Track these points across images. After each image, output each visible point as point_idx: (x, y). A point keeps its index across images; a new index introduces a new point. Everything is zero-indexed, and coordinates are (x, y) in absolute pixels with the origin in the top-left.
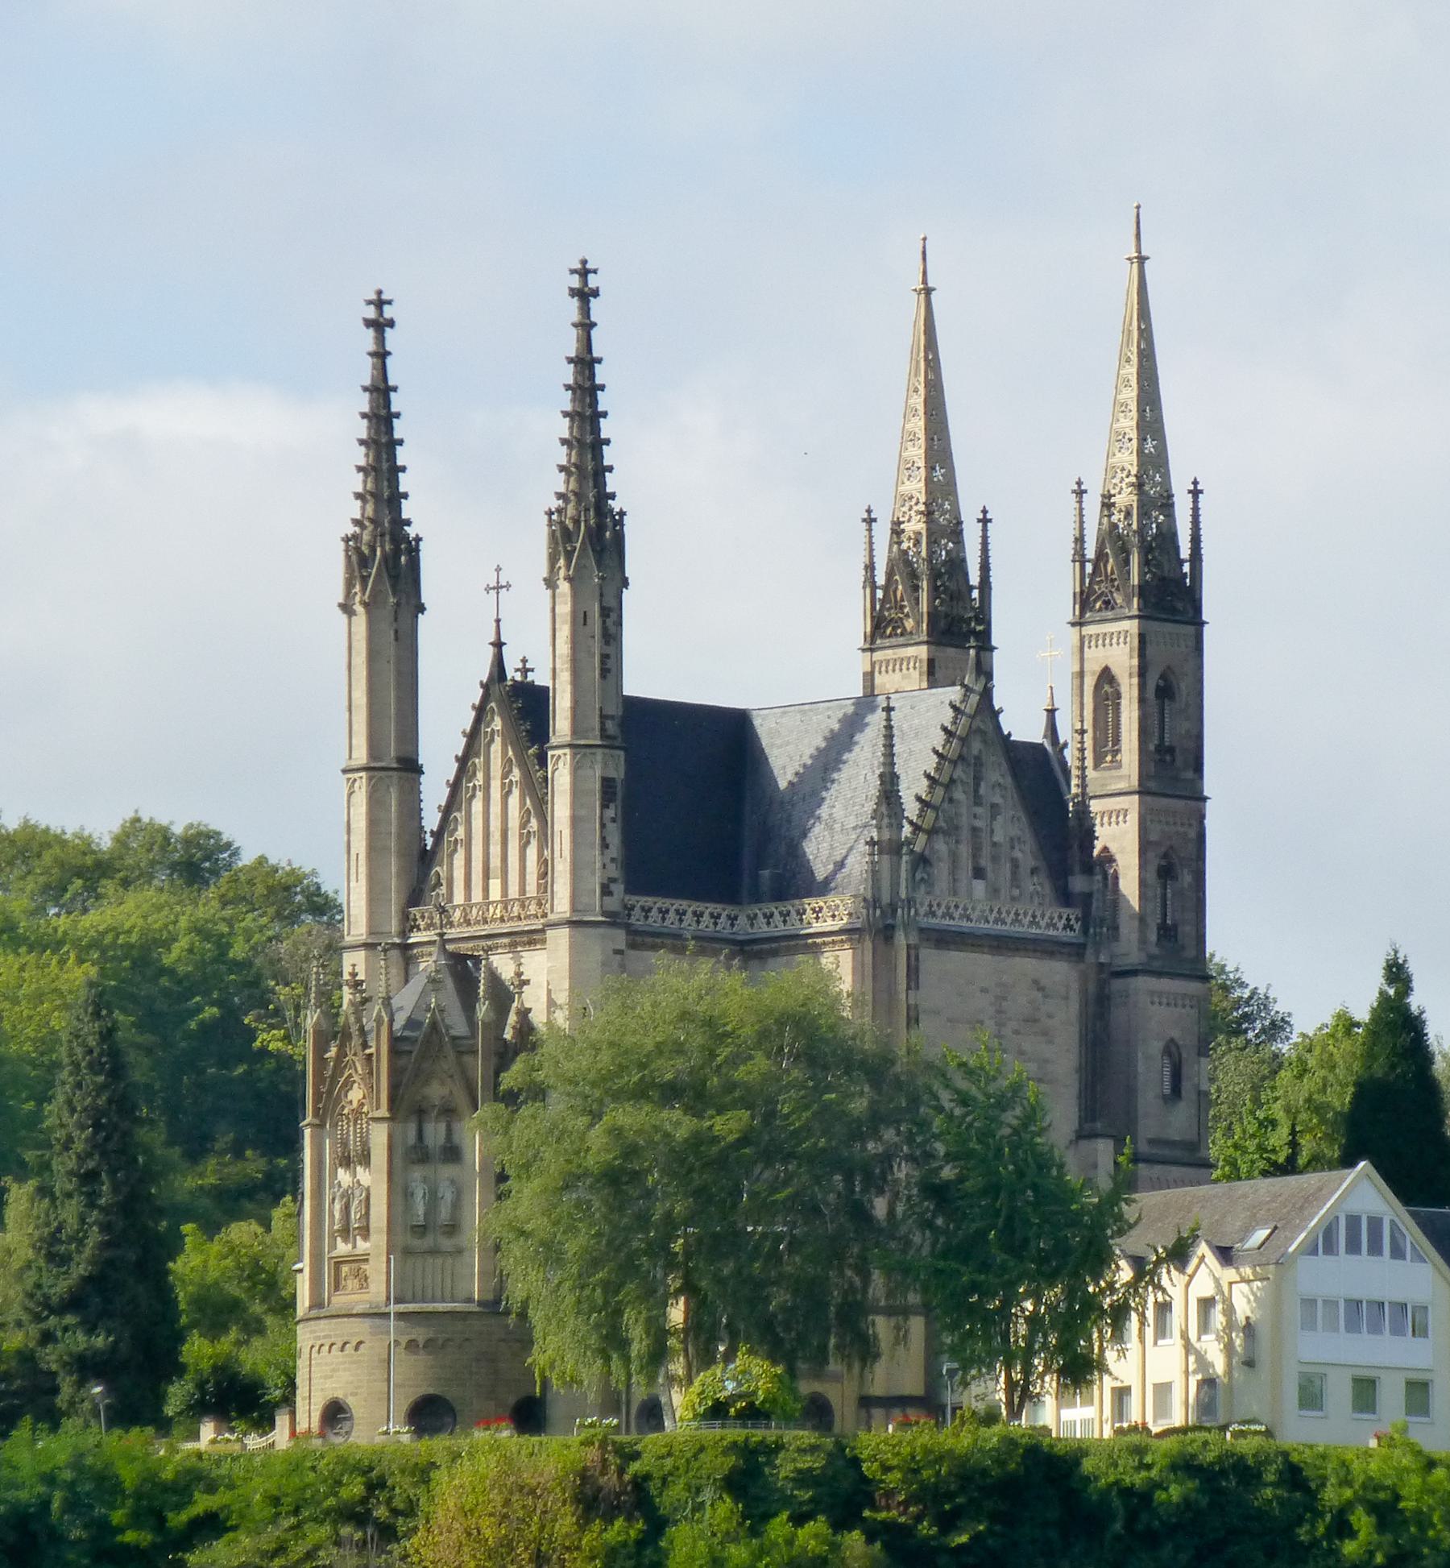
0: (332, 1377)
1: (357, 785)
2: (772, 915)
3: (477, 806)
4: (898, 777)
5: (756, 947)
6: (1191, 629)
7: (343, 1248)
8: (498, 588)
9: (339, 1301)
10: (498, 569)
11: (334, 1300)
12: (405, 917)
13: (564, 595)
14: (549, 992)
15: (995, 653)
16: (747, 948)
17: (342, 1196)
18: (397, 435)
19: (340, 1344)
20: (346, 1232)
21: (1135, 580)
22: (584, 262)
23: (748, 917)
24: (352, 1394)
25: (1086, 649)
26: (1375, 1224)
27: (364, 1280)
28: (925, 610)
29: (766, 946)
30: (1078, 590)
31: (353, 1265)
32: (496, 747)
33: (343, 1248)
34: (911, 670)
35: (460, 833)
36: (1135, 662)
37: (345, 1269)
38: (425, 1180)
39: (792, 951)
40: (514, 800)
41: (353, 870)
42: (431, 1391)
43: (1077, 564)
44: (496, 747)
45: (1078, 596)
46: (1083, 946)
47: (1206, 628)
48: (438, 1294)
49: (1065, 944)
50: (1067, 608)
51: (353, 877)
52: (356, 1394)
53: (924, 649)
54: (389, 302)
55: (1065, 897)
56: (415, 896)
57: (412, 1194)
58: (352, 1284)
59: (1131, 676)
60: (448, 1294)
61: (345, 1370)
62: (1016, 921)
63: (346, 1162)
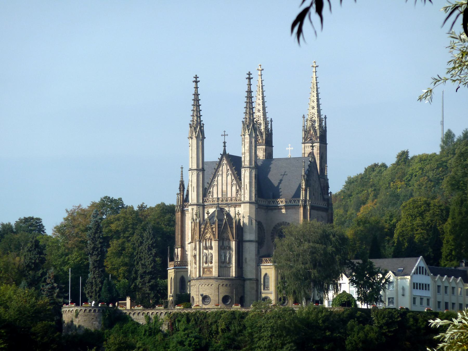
0: (205, 291)
1: (194, 173)
2: (270, 202)
3: (220, 178)
4: (349, 178)
5: (271, 208)
6: (325, 145)
7: (205, 265)
8: (225, 135)
9: (205, 276)
10: (225, 132)
11: (203, 276)
12: (203, 200)
13: (247, 138)
14: (243, 215)
15: (273, 147)
16: (268, 208)
17: (206, 255)
18: (200, 104)
19: (221, 285)
20: (206, 263)
21: (318, 135)
22: (249, 72)
23: (268, 202)
24: (210, 294)
25: (306, 148)
26: (423, 268)
27: (211, 272)
28: (264, 138)
29: (273, 208)
30: (304, 136)
31: (208, 269)
32: (225, 167)
33: (205, 265)
34: (261, 150)
35: (215, 183)
36: (319, 151)
37: (205, 270)
38: (224, 253)
39: (275, 209)
40: (229, 177)
41: (193, 190)
42: (227, 294)
43: (304, 132)
44: (225, 167)
45: (304, 138)
46: (328, 209)
47: (327, 145)
48: (226, 275)
49: (263, 206)
50: (301, 140)
51: (193, 191)
52: (211, 294)
53: (264, 146)
54: (198, 77)
55: (324, 199)
56: (204, 195)
57: (222, 255)
58: (208, 273)
59: (317, 154)
60: (228, 275)
61: (208, 290)
62: (316, 204)
63: (206, 248)
